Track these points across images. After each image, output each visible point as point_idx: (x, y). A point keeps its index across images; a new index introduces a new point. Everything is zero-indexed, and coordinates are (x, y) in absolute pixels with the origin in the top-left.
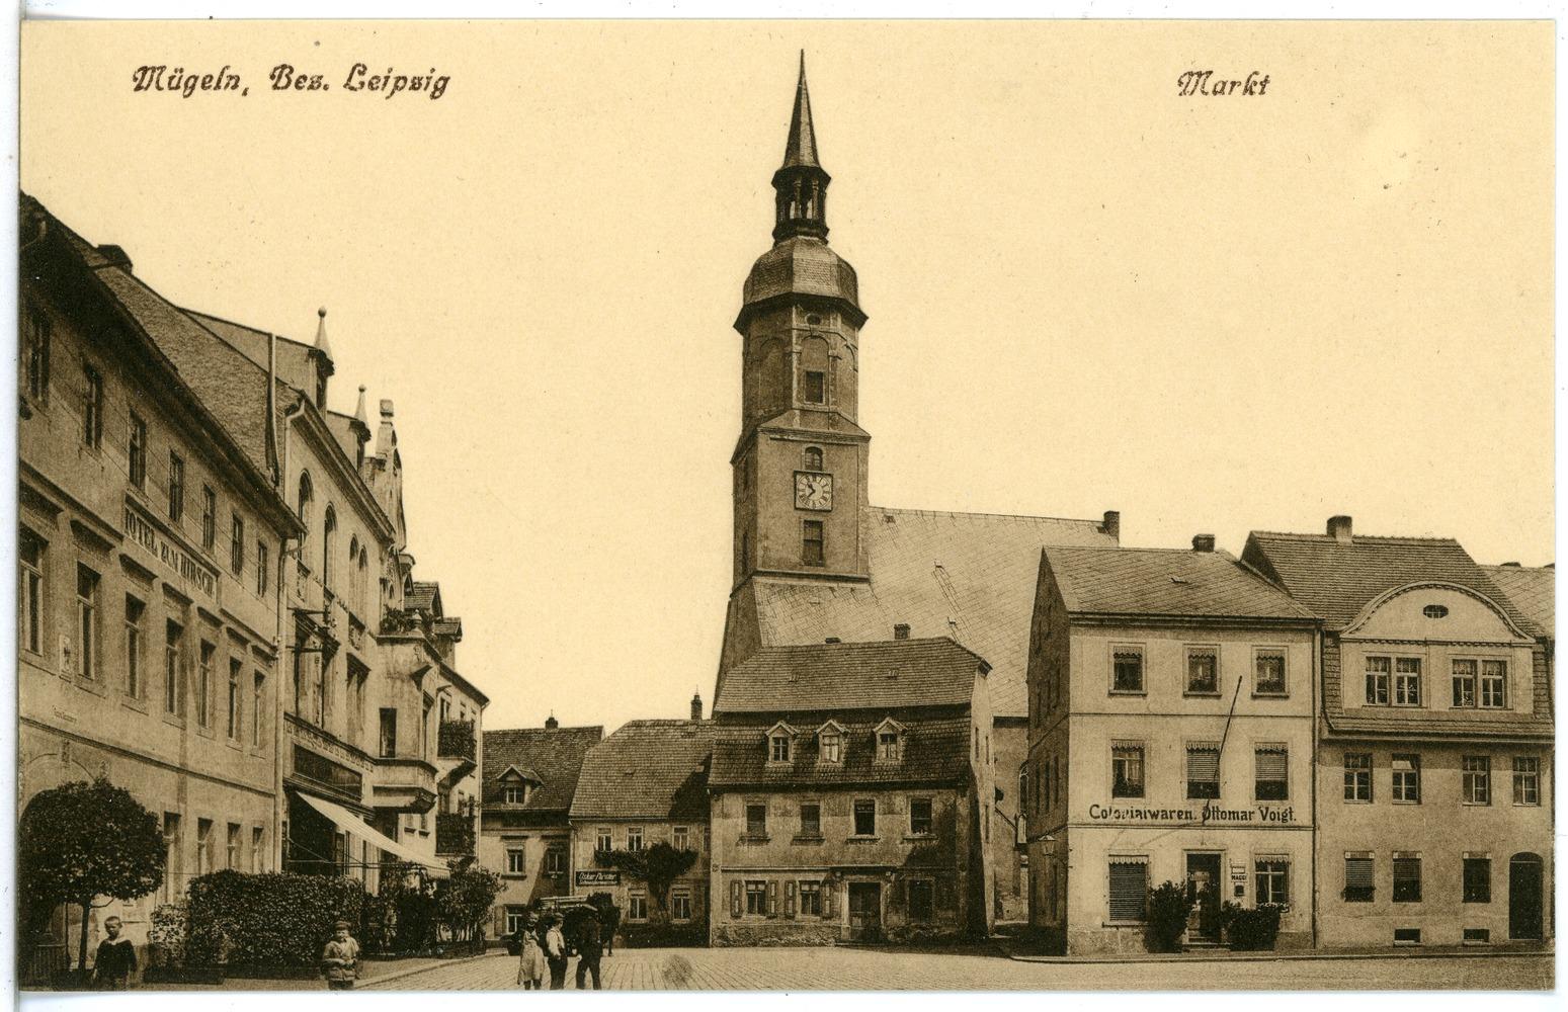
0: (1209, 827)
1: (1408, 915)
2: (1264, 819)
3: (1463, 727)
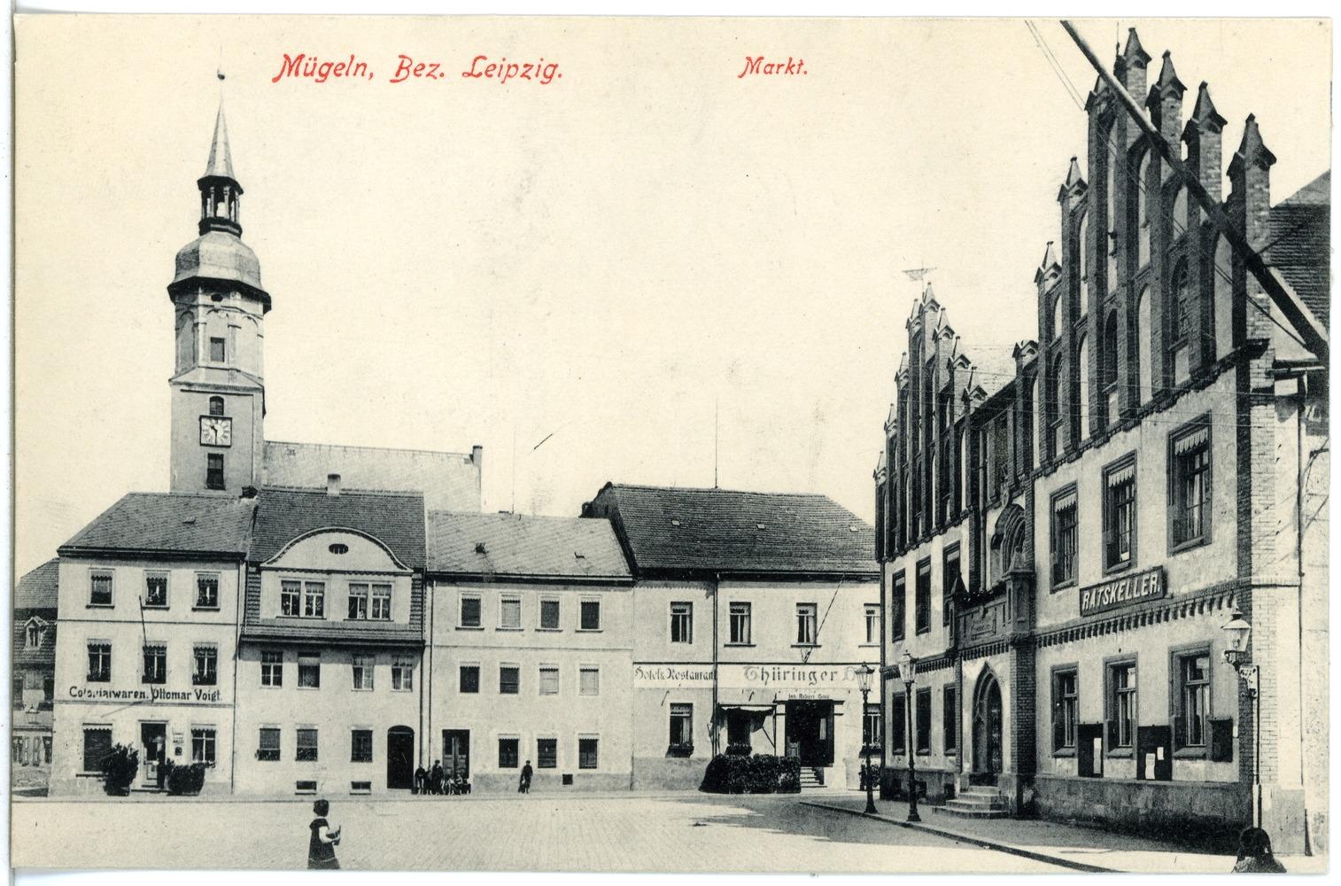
0: (157, 704)
1: (306, 771)
2: (198, 698)
3: (287, 632)
